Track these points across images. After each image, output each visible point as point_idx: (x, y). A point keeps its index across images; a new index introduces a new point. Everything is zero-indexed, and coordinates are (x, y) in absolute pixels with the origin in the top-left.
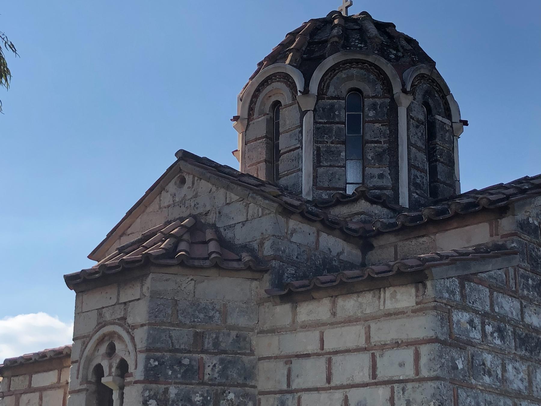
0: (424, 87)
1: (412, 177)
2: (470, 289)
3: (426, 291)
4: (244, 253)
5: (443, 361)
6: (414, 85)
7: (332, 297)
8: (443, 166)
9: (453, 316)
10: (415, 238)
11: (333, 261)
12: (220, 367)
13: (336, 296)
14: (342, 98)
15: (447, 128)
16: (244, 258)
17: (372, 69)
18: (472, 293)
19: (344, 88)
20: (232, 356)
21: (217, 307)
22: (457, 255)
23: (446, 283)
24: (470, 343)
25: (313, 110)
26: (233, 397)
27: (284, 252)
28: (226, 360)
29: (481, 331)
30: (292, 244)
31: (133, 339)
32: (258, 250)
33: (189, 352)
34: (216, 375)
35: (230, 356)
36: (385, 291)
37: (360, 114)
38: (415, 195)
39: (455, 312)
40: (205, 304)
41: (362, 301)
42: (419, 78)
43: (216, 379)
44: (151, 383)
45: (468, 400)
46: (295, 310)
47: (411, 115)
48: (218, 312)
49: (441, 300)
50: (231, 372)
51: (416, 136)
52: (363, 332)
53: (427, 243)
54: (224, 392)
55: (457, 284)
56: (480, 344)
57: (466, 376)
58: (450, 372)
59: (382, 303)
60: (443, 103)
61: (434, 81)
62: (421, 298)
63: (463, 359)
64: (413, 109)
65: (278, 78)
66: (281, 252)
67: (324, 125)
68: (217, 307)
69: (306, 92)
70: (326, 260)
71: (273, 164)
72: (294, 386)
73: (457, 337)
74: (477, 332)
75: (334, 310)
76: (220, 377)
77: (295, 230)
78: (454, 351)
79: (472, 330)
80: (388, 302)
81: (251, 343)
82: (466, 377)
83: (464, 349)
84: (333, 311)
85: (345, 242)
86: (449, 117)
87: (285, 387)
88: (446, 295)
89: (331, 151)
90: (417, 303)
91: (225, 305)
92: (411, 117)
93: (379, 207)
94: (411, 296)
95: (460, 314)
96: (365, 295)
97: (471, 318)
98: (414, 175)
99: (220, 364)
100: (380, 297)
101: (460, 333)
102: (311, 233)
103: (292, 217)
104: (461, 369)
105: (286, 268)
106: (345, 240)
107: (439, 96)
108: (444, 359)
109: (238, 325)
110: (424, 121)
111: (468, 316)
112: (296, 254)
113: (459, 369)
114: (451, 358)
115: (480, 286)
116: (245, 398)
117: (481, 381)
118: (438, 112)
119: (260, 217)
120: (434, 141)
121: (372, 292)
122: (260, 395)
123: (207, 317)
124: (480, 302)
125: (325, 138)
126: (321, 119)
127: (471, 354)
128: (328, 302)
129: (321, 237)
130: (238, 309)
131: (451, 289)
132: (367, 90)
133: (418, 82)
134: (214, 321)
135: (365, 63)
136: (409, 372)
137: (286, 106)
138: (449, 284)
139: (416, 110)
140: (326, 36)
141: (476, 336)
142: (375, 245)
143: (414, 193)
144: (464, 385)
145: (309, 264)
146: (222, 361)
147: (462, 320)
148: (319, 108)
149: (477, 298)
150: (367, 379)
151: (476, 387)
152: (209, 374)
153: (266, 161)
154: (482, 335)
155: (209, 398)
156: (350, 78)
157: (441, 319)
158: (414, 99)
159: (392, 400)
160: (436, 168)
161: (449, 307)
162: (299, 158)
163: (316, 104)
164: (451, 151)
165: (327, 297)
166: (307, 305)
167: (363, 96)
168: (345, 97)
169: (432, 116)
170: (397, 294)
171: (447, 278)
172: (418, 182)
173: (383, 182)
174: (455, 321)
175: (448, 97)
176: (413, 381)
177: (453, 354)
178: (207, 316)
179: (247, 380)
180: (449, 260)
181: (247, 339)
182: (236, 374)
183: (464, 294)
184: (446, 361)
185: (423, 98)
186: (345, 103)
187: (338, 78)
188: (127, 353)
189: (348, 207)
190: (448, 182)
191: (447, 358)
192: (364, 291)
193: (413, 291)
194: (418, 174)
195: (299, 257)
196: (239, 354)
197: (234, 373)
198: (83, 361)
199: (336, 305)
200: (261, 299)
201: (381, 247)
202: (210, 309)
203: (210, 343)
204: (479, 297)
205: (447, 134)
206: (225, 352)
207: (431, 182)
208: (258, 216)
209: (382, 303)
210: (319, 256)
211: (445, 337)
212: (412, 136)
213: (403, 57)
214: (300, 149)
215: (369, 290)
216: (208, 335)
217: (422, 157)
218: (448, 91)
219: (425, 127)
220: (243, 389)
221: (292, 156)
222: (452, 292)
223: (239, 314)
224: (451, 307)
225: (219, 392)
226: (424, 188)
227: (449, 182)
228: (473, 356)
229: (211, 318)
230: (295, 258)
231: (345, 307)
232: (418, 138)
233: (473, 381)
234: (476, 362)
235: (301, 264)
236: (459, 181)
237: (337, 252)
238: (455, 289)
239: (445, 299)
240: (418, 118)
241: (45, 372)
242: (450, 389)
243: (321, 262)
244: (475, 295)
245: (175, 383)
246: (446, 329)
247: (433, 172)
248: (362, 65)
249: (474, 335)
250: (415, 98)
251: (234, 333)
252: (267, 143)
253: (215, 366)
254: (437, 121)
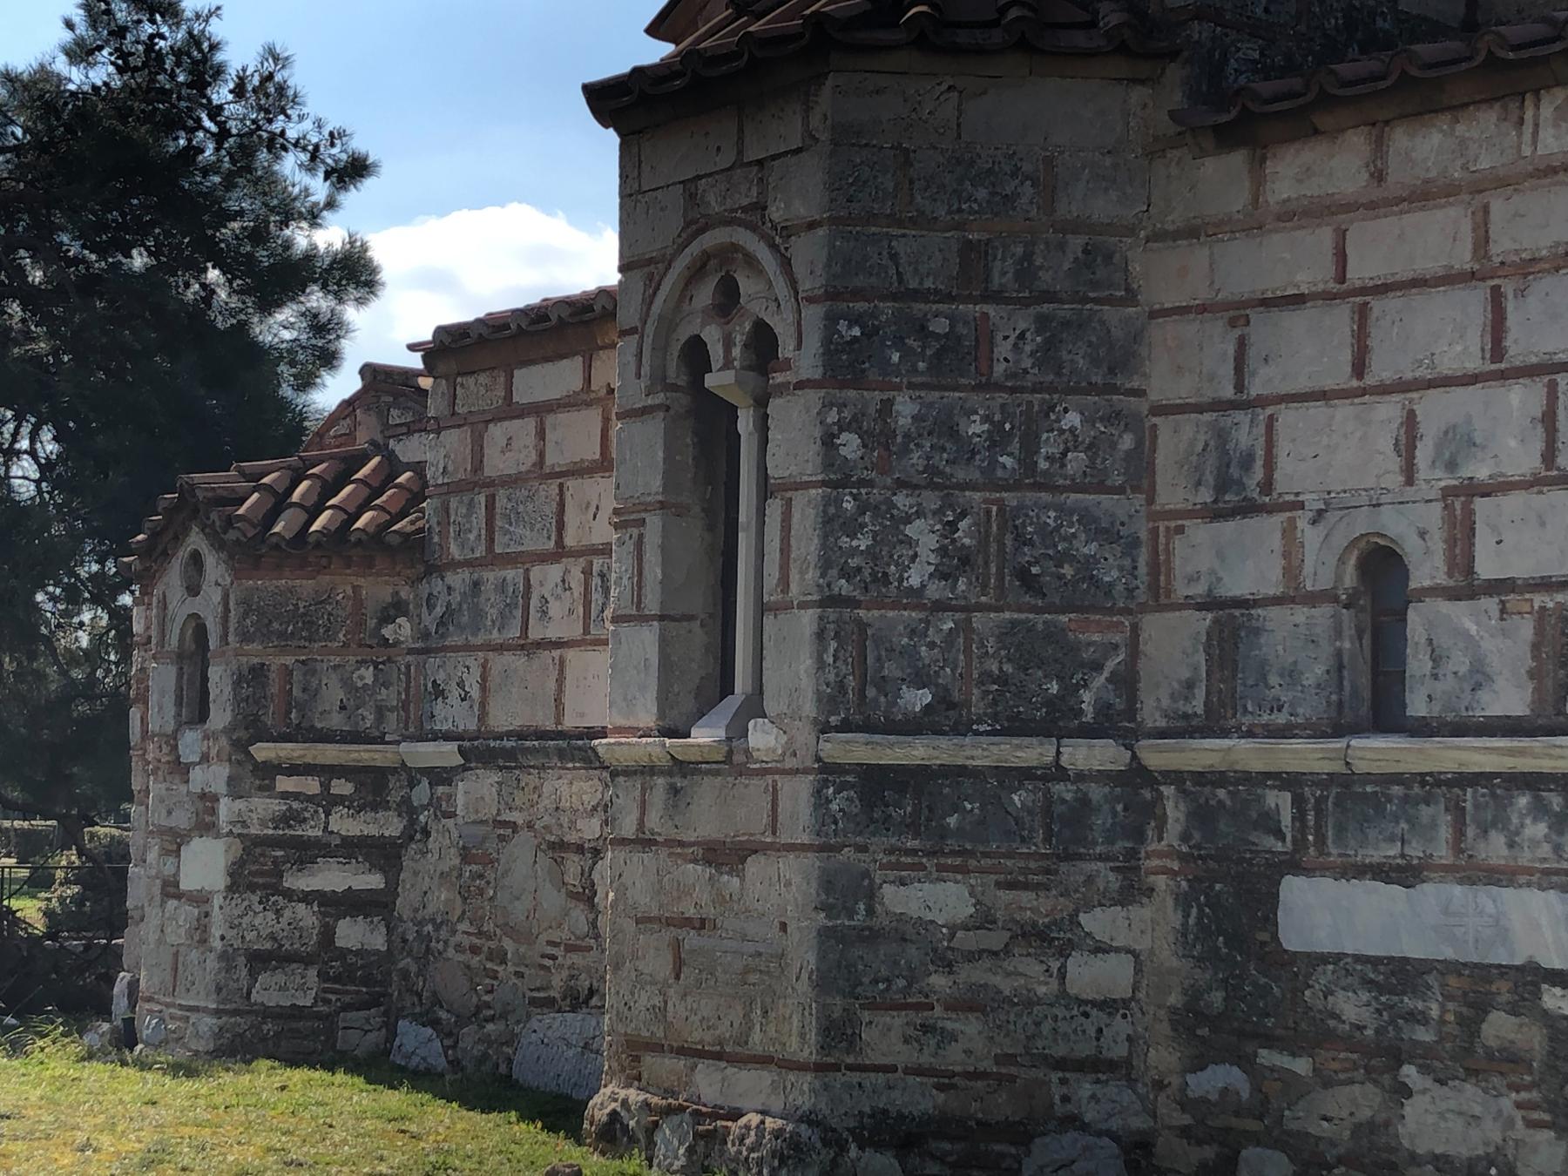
31: (786, 264)
33: (950, 298)
44: (843, 385)
72: (1255, 389)
100: (1521, 121)
146: (1042, 322)
188: (773, 306)
198: (650, 329)
206: (1049, 296)
241: (547, 360)
245: (911, 386)
253: (1022, 336)
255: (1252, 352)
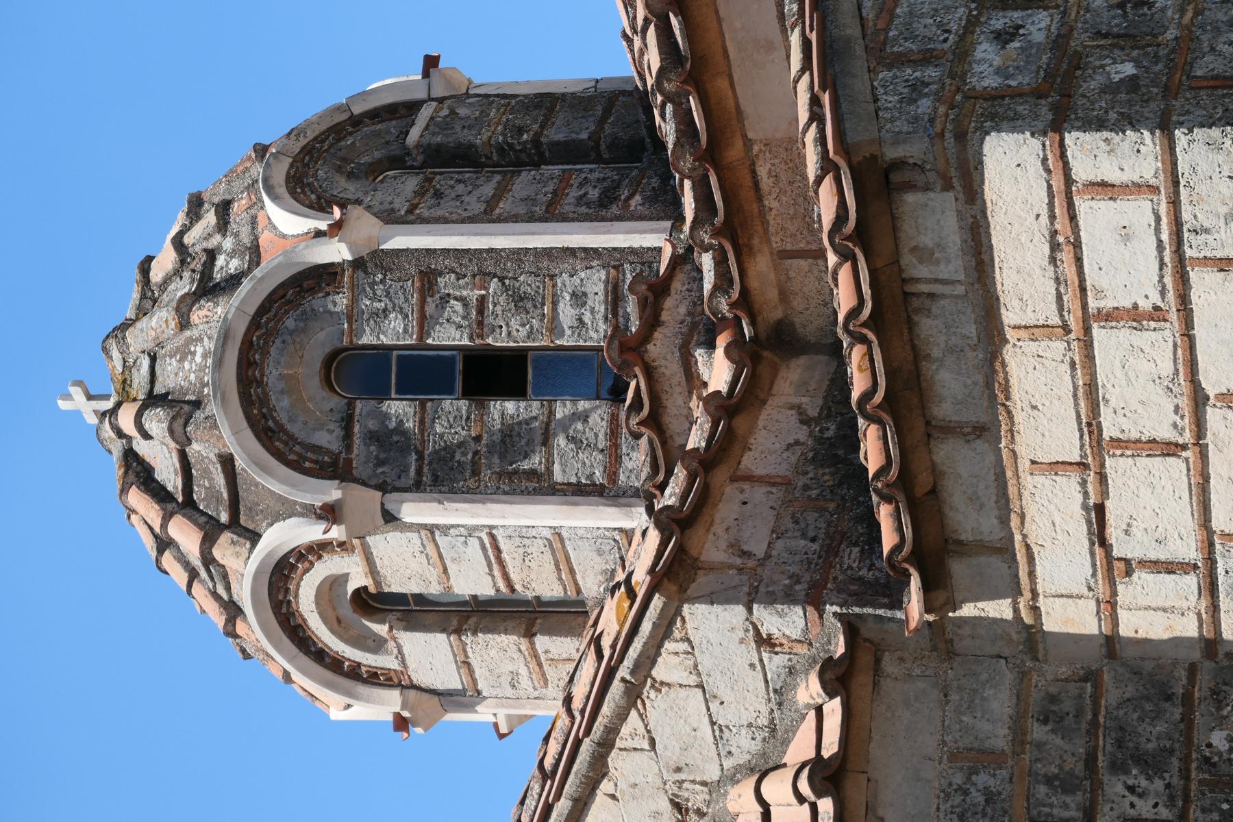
0: (325, 176)
1: (583, 210)
2: (906, 39)
3: (911, 161)
4: (798, 698)
5: (1113, 116)
6: (319, 202)
7: (929, 436)
8: (553, 124)
9: (985, 88)
10: (760, 198)
11: (825, 436)
12: (1134, 772)
13: (928, 423)
14: (349, 409)
15: (445, 112)
16: (815, 696)
17: (267, 323)
18: (917, 33)
19: (329, 403)
20: (1104, 736)
21: (958, 779)
22: (808, 73)
23: (889, 105)
24: (1059, 42)
25: (381, 494)
26: (1224, 733)
27: (796, 579)
28: (1114, 756)
29: (1027, 9)
30: (774, 553)
32: (790, 653)
34: (1159, 784)
35: (1104, 742)
36: (913, 279)
37: (399, 357)
38: (633, 203)
39: (973, 81)
40: (949, 816)
41: (942, 346)
42: (298, 190)
43: (1169, 783)
45: (1226, 49)
46: (967, 545)
47: (403, 212)
48: (974, 778)
49: (938, 120)
50: (1148, 740)
51: (466, 199)
52: (1030, 347)
53: (773, 165)
54: (1207, 760)
55: (891, 74)
56: (1064, 13)
57: (1156, 55)
58: (1146, 97)
59: (946, 290)
60: (373, 124)
61: (309, 147)
62: (932, 176)
63: (1108, 61)
64: (387, 206)
65: (285, 597)
66: (798, 587)
67: (426, 462)
68: (958, 779)
69: (330, 513)
70: (820, 457)
71: (537, 615)
72: (1189, 551)
73: (1045, 77)
74: (1030, 21)
75: (966, 430)
76: (1165, 774)
77: (731, 546)
78: (1085, 85)
79: (1024, 35)
80: (944, 272)
81: (1067, 680)
82: (1161, 53)
83: (1081, 58)
84: (969, 434)
85: (770, 402)
86: (412, 107)
87: (1190, 582)
88: (925, 105)
89: (503, 442)
90: (948, 187)
91: (953, 757)
92: (410, 211)
93: (669, 303)
94: (926, 205)
95: (977, 68)
96: (922, 337)
97: (992, 36)
98: (578, 204)
99: (1127, 772)
100: (932, 296)
101: (1034, 68)
102: (742, 497)
103: (694, 552)
104: (1137, 67)
105: (844, 572)
106: (764, 402)
107: (351, 134)
108: (1106, 112)
109: (1011, 718)
110: (421, 176)
111: (985, 46)
112: (803, 543)
113: (1135, 72)
114: (1105, 93)
115: (898, 11)
116: (1225, 698)
117: (1170, 13)
118: (398, 137)
119: (693, 648)
120: (480, 149)
121: (916, 318)
122: (1216, 655)
123: (989, 810)
124: (942, 11)
125: (463, 459)
126: (409, 470)
127: (1092, 39)
128: (944, 446)
129: (754, 469)
130: (964, 719)
131: (906, 90)
132: (320, 342)
133: (309, 193)
134: (1000, 789)
135: (252, 342)
136: (1139, 212)
137: (373, 570)
138: (893, 95)
139: (390, 199)
140: (167, 455)
141: (1043, 25)
142: (778, 314)
143: (629, 206)
144: (1183, 60)
145: (832, 506)
146: (1117, 767)
147: (995, 63)
148: (376, 475)
149: (931, 21)
150: (1170, 332)
151: (1187, 27)
152: (1156, 805)
153: (530, 635)
154: (1038, 8)
155: (1225, 806)
156: (291, 386)
157: (992, 120)
158: (358, 202)
159: (1224, 264)
160: (558, 143)
161: (958, 98)
162: (522, 534)
163: (364, 484)
164: (509, 103)
165: (930, 450)
166: (951, 508)
167: (346, 349)
168: (346, 401)
169: (408, 154)
170: (921, 245)
171: (876, 100)
172: (597, 195)
173: (596, 294)
174: (1000, 80)
175: (357, 110)
176: (1175, 203)
177: (1093, 90)
178: (983, 810)
179: (1173, 694)
180: (821, 94)
181: (1053, 690)
182: (1154, 727)
183: (921, 57)
184: (1113, 108)
185: (357, 178)
186: (363, 401)
187: (291, 420)
189: (667, 392)
190: (599, 110)
191: (1104, 105)
192: (912, 340)
193: (911, 198)
194: (574, 193)
195: (811, 534)
196: (1096, 715)
197: (1154, 732)
199: (952, 425)
200: (934, 648)
201: (784, 296)
202: (964, 800)
203: (1064, 802)
204: (930, 16)
205: (462, 111)
206: (1090, 760)
207: (599, 160)
208: (688, 653)
209: (946, 290)
210: (811, 475)
211: (1044, 110)
212: (466, 210)
213: (237, 235)
214: (494, 532)
215: (911, 325)
216: (1043, 809)
217: (524, 183)
218: (339, 108)
219: (441, 174)
220: (1199, 704)
221: (516, 555)
222: (913, 87)
223: (979, 715)
224: (958, 89)
225: (1207, 776)
226: (616, 177)
227: (600, 108)
228: (1099, 34)
229: (990, 796)
230: (815, 546)
231: (959, 397)
232: (470, 192)
233: (1171, 34)
234: (1117, 25)
235: (832, 529)
236: (597, 81)
237: (798, 425)
238: (907, 81)
239: (935, 109)
240: (415, 192)
242: (1195, 98)
243: (827, 470)
244: (925, 26)
246: (1022, 107)
247: (570, 153)
248: (256, 351)
249: (1040, 29)
250: (357, 200)
251: (1038, 732)
252: (475, 633)
253: (1131, 789)
254: (425, 141)
255: (1153, 556)
